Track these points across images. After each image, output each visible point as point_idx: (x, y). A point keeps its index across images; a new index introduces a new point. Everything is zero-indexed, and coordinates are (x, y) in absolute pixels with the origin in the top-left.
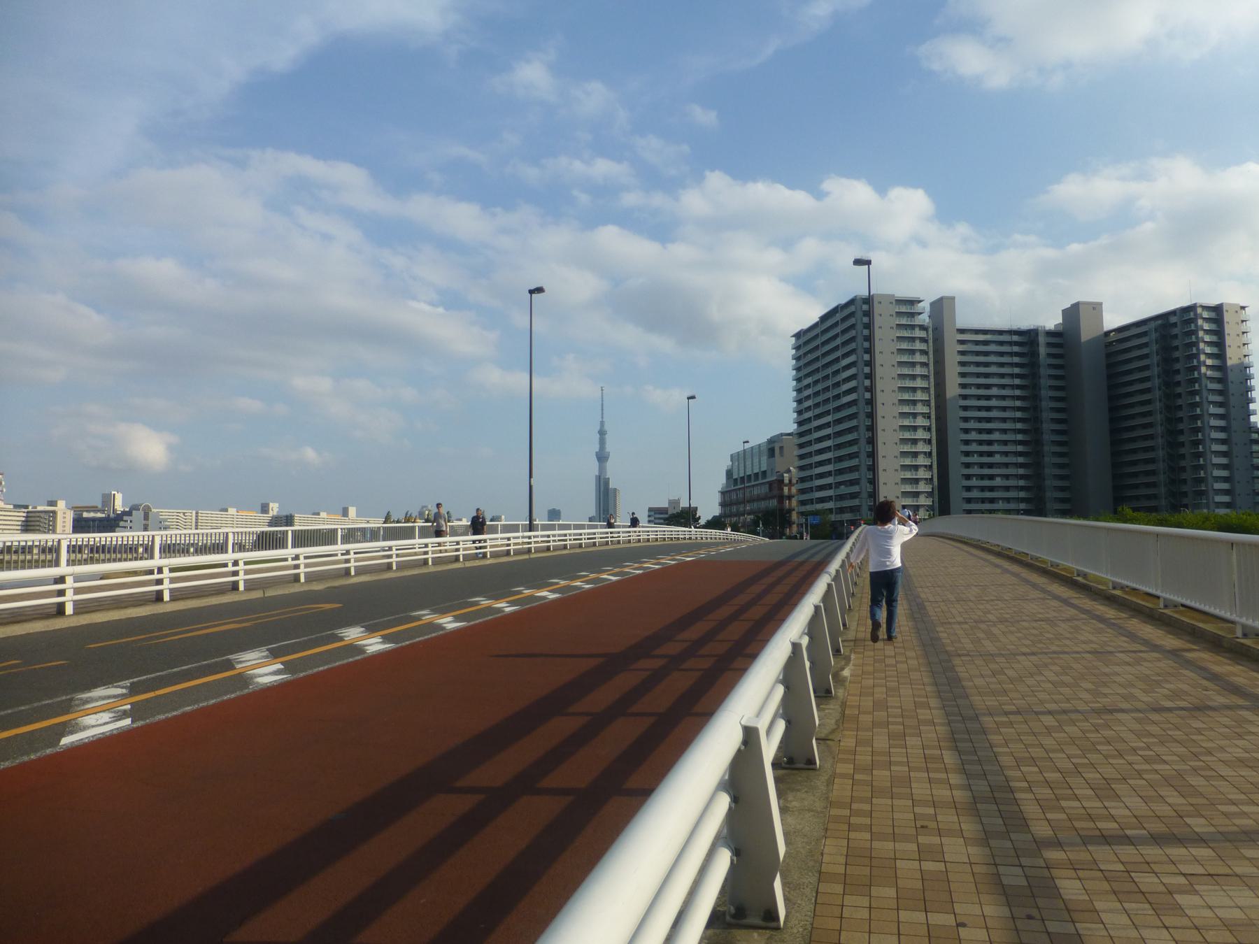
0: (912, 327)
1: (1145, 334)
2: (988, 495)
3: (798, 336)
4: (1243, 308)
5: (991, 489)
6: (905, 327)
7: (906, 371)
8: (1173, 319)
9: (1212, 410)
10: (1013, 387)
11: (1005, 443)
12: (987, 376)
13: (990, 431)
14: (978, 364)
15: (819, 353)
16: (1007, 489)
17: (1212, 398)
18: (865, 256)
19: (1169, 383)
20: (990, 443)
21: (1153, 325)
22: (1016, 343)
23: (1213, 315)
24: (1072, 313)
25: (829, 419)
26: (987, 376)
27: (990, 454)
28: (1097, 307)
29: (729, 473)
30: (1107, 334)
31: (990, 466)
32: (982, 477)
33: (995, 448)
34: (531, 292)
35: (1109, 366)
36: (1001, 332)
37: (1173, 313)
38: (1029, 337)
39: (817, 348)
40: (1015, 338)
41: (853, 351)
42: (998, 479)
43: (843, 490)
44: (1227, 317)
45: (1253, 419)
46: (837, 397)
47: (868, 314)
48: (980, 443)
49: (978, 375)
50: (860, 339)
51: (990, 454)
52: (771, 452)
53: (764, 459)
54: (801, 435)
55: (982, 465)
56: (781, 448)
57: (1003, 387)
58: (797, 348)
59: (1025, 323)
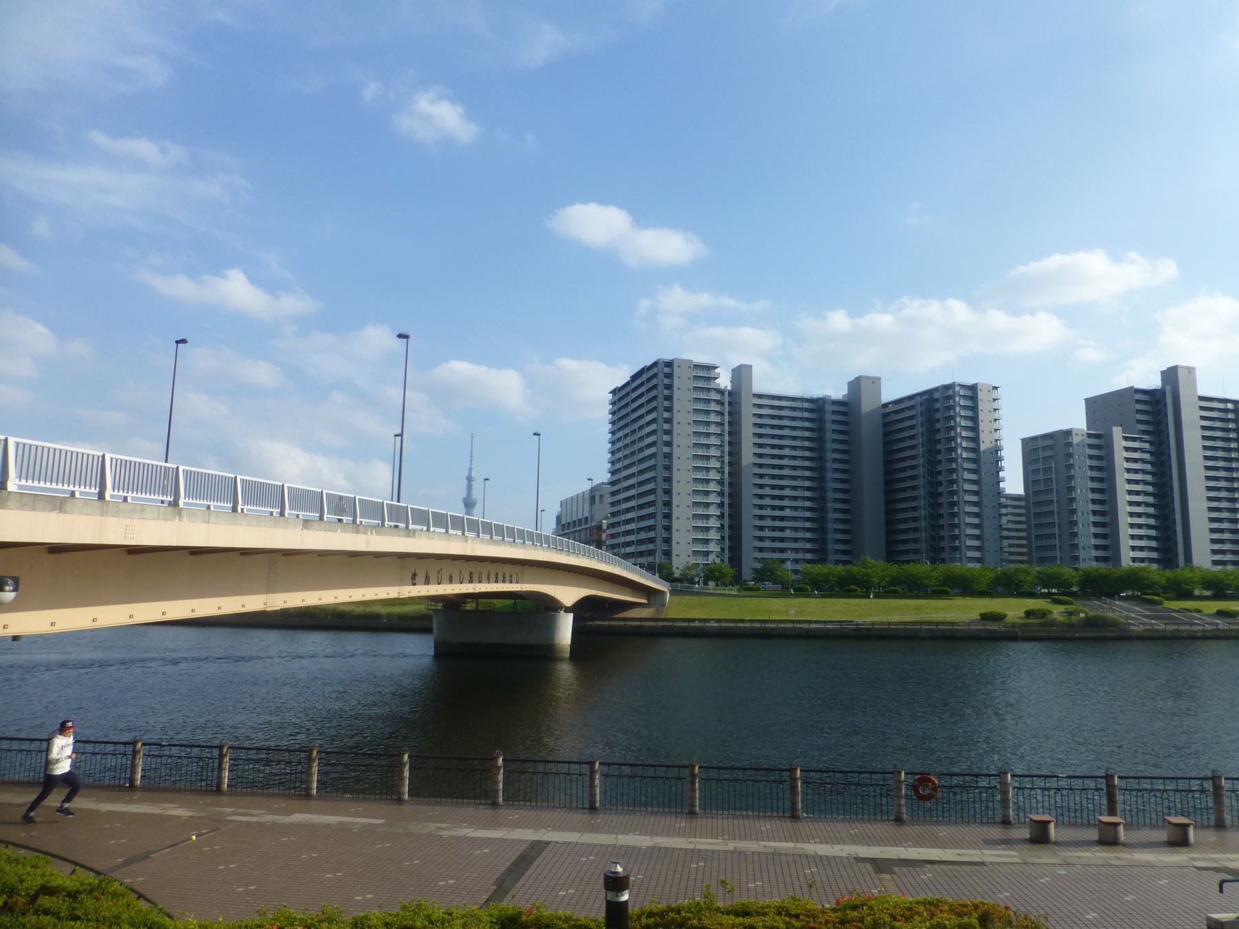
0: (709, 390)
1: (911, 408)
2: (778, 545)
3: (614, 392)
4: (995, 388)
5: (782, 540)
6: (702, 389)
7: (702, 429)
8: (936, 395)
9: (967, 476)
10: (803, 448)
11: (795, 498)
12: (781, 437)
13: (782, 488)
14: (773, 427)
15: (629, 409)
16: (796, 540)
17: (966, 465)
18: (404, 331)
19: (932, 452)
20: (782, 498)
21: (919, 399)
22: (807, 410)
23: (969, 393)
24: (856, 385)
25: (633, 470)
26: (781, 437)
27: (782, 508)
28: (876, 381)
29: (559, 519)
30: (885, 405)
31: (782, 519)
32: (774, 529)
33: (786, 503)
34: (177, 342)
35: (886, 434)
36: (794, 399)
37: (936, 389)
38: (818, 406)
39: (627, 404)
40: (806, 405)
41: (654, 409)
42: (788, 531)
43: (643, 535)
44: (981, 395)
45: (1002, 485)
46: (641, 450)
47: (669, 376)
48: (773, 497)
49: (773, 437)
50: (660, 398)
51: (782, 508)
52: (593, 499)
53: (587, 505)
54: (613, 483)
55: (774, 518)
56: (601, 496)
57: (794, 448)
58: (613, 403)
59: (816, 392)
